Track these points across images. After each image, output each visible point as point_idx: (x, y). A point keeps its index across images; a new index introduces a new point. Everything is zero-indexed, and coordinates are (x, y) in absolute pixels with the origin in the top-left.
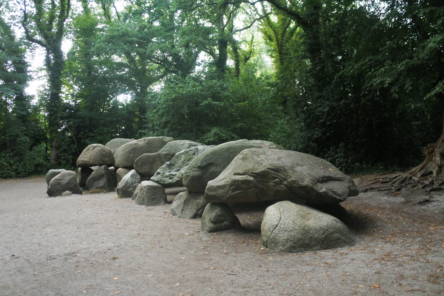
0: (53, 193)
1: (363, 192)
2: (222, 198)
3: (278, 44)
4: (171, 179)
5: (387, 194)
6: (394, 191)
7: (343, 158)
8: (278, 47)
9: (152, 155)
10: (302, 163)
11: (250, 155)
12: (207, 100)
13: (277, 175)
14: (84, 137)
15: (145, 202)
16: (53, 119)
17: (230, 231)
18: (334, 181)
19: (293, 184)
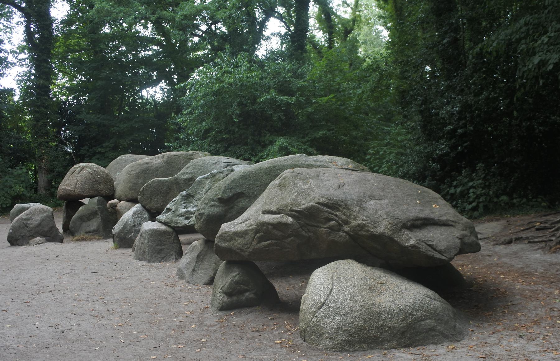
0: (17, 240)
1: (504, 244)
2: (242, 253)
3: (396, 7)
4: (187, 218)
5: (542, 248)
6: (553, 244)
7: (481, 187)
8: (397, 11)
9: (167, 181)
10: (382, 194)
11: (291, 179)
12: (269, 93)
13: (332, 214)
14: (89, 154)
15: (147, 256)
16: (41, 126)
17: (255, 309)
18: (435, 227)
19: (360, 231)
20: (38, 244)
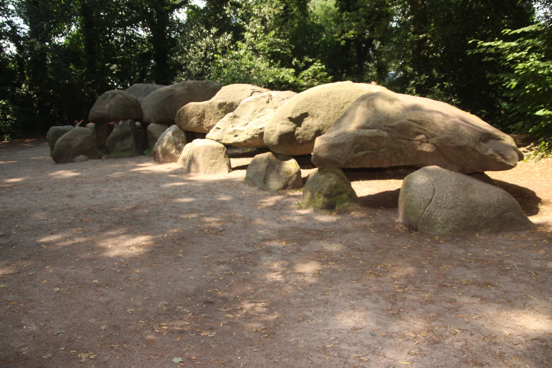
20: (82, 161)
